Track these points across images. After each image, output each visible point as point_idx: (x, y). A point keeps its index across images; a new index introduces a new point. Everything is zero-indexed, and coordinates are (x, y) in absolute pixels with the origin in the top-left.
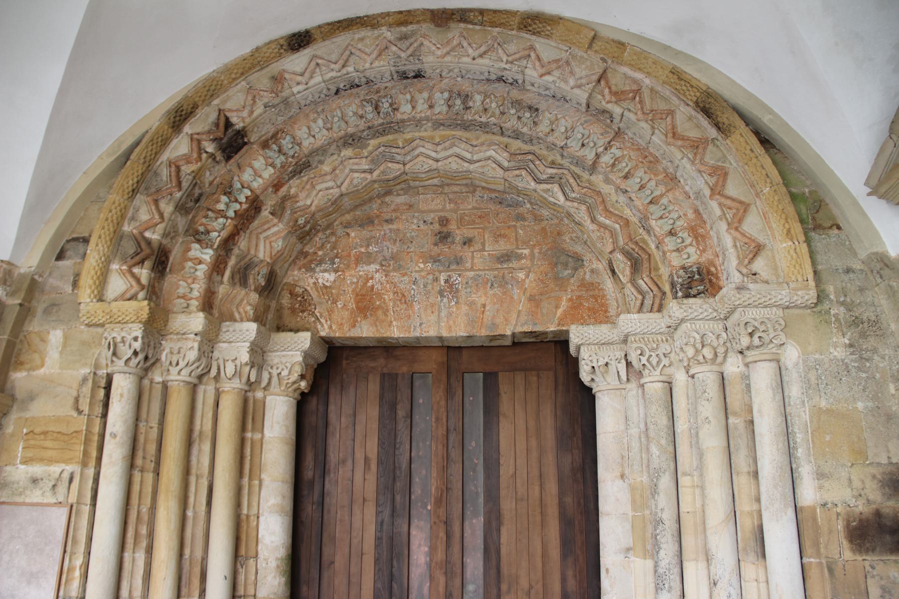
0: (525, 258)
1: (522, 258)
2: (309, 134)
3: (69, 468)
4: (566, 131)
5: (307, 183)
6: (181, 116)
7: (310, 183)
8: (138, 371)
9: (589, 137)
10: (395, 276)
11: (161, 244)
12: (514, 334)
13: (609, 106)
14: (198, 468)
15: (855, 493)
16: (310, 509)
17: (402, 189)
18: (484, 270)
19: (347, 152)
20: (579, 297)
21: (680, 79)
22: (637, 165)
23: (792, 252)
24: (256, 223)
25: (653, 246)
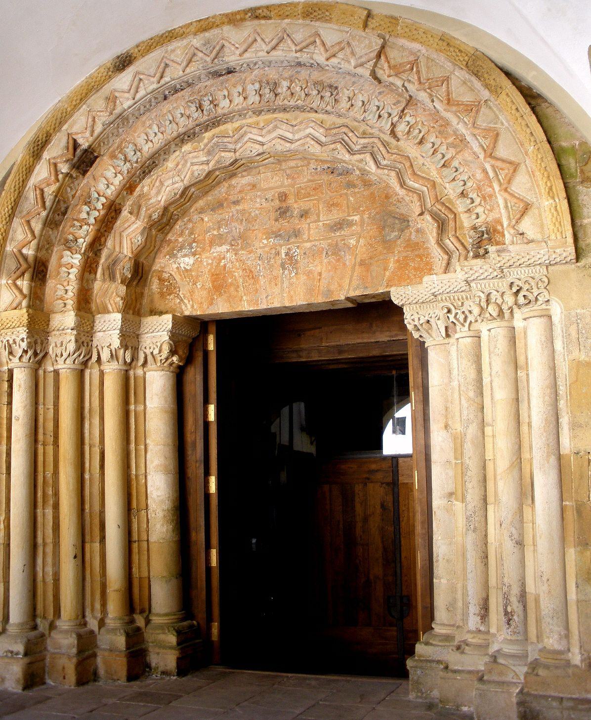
0: (355, 224)
18: (320, 240)
19: (187, 147)
22: (429, 131)
23: (553, 210)
24: (118, 222)
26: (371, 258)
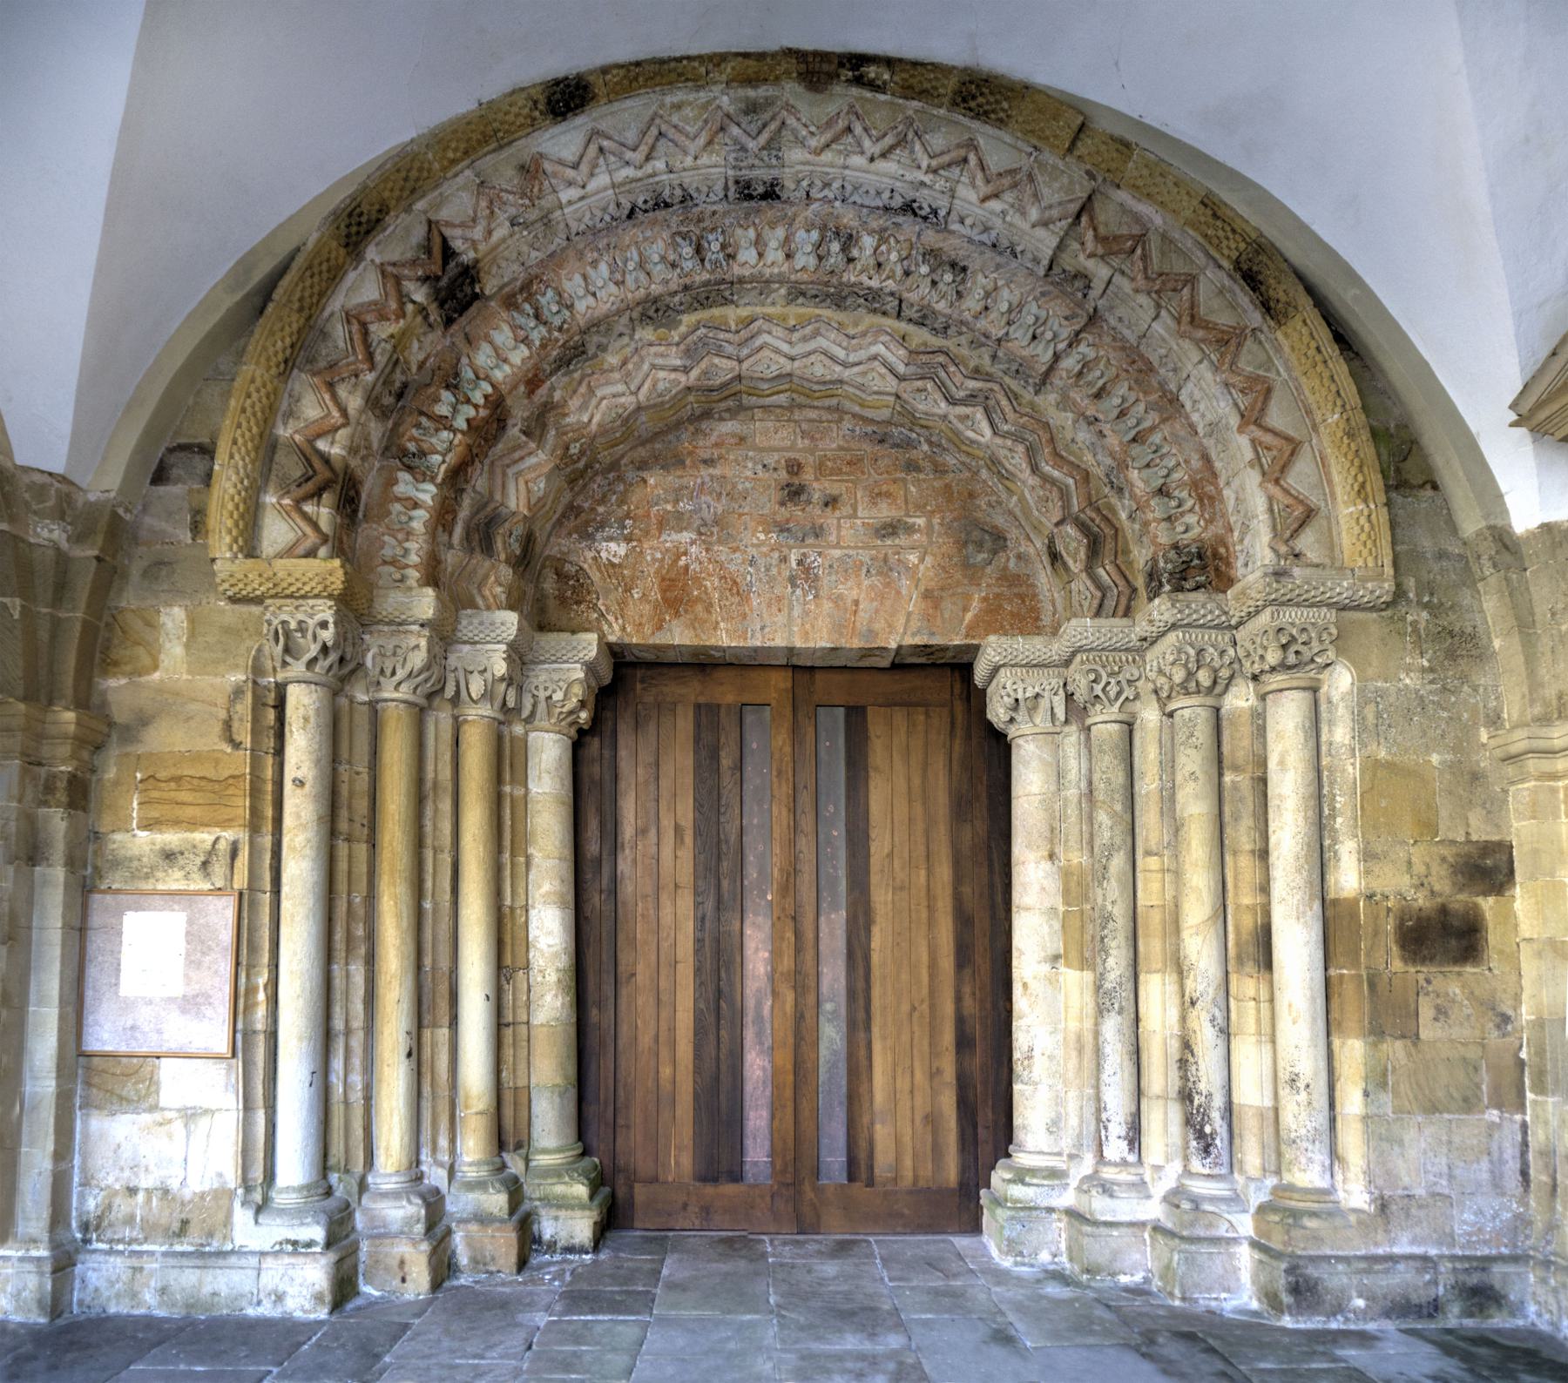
0: (919, 531)
1: (915, 531)
2: (591, 290)
3: (229, 835)
4: (1010, 311)
5: (580, 383)
6: (359, 224)
7: (584, 384)
8: (330, 679)
9: (1044, 323)
10: (722, 552)
11: (347, 466)
12: (900, 647)
13: (1090, 265)
14: (435, 838)
15: (1415, 881)
16: (596, 899)
17: (728, 410)
18: (856, 547)
19: (646, 334)
20: (997, 596)
21: (1215, 216)
23: (1363, 520)
25: (1123, 516)
26: (942, 589)
